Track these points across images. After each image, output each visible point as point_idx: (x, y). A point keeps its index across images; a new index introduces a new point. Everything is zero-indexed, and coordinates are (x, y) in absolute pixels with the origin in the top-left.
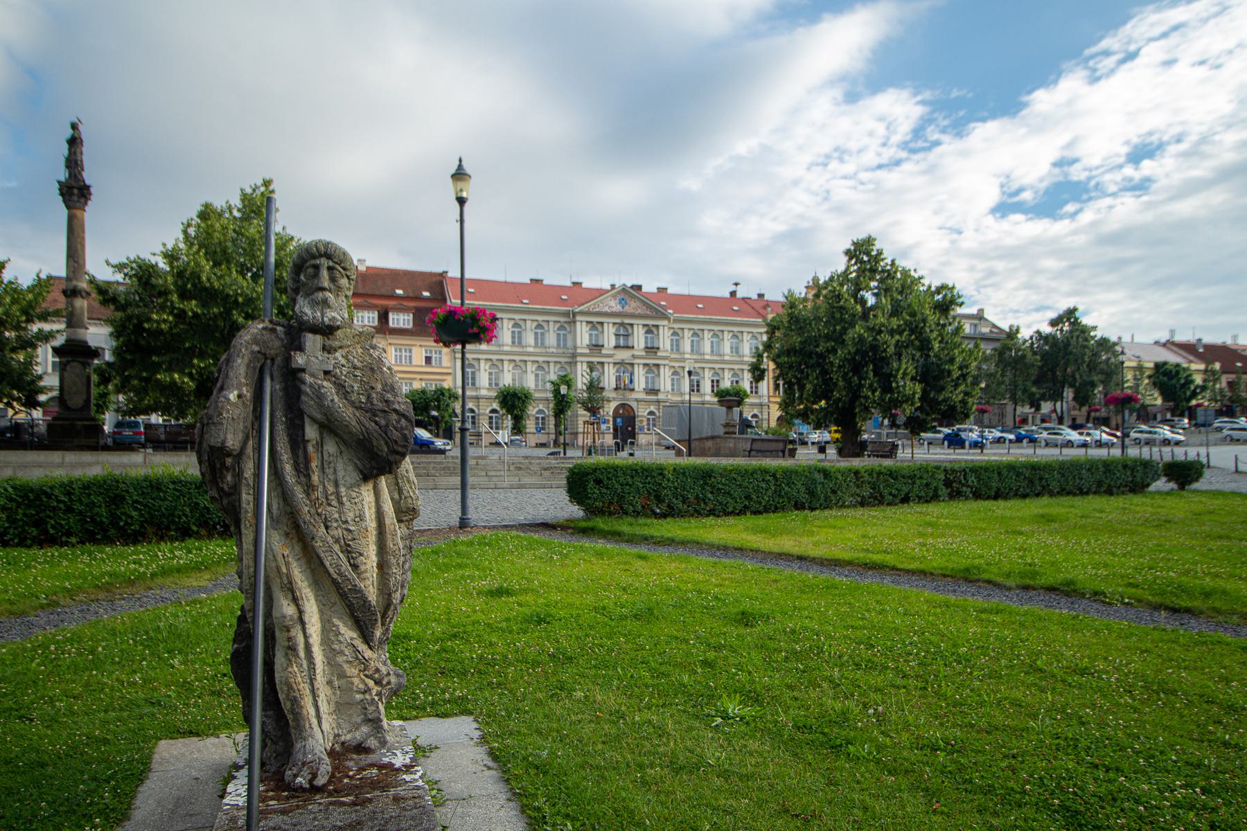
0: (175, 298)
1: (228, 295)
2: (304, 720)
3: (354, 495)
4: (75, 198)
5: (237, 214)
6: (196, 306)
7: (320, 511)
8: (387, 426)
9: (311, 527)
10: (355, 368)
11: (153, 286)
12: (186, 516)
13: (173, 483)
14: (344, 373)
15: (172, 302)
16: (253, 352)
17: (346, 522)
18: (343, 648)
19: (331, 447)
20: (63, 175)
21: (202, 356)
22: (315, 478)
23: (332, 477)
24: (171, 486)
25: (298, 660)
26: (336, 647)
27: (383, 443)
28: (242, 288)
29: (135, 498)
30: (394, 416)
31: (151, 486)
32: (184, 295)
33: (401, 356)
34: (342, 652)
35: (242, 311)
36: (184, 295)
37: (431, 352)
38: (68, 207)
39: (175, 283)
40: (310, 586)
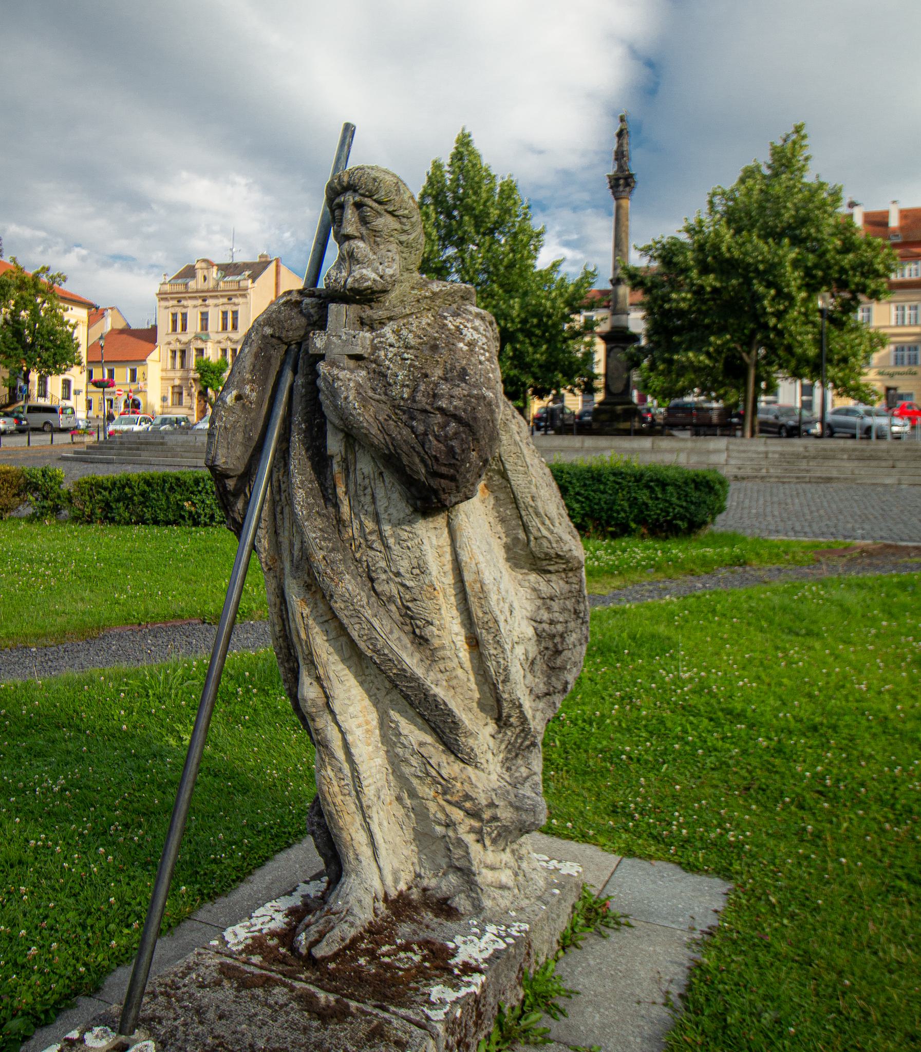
0: (694, 273)
1: (749, 264)
2: (347, 848)
3: (405, 535)
4: (621, 189)
5: (767, 172)
6: (715, 279)
7: (358, 555)
8: (425, 434)
9: (327, 580)
10: (407, 347)
11: (676, 264)
12: (625, 512)
13: (615, 474)
14: (390, 355)
15: (691, 279)
16: (264, 337)
17: (398, 574)
18: (408, 756)
21: (720, 332)
22: (345, 509)
23: (370, 509)
24: (612, 478)
25: (334, 761)
26: (399, 751)
27: (417, 460)
28: (762, 253)
29: (577, 489)
30: (439, 418)
31: (593, 478)
32: (705, 270)
34: (406, 761)
35: (763, 280)
36: (705, 270)
38: (617, 199)
39: (696, 260)
40: (343, 660)
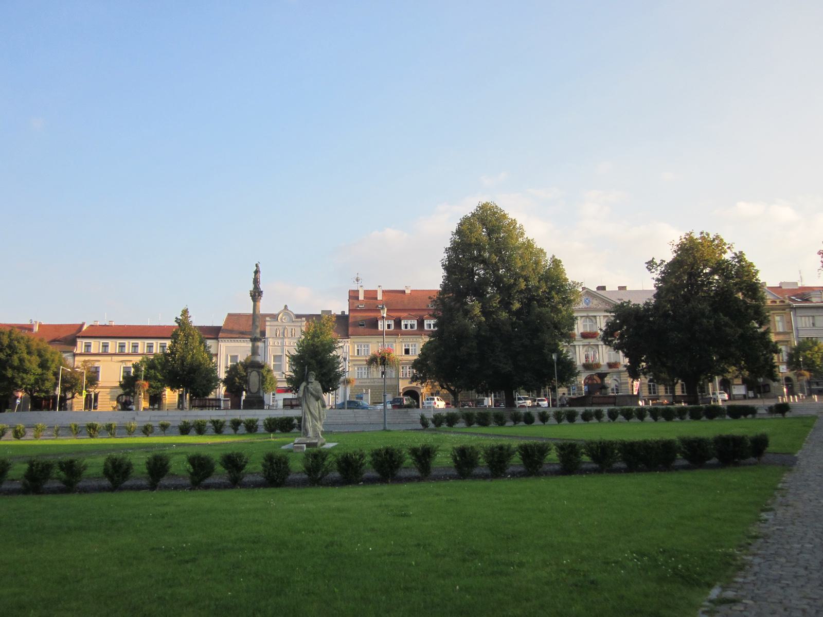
19: (312, 397)
20: (251, 287)
33: (361, 373)
37: (408, 346)
